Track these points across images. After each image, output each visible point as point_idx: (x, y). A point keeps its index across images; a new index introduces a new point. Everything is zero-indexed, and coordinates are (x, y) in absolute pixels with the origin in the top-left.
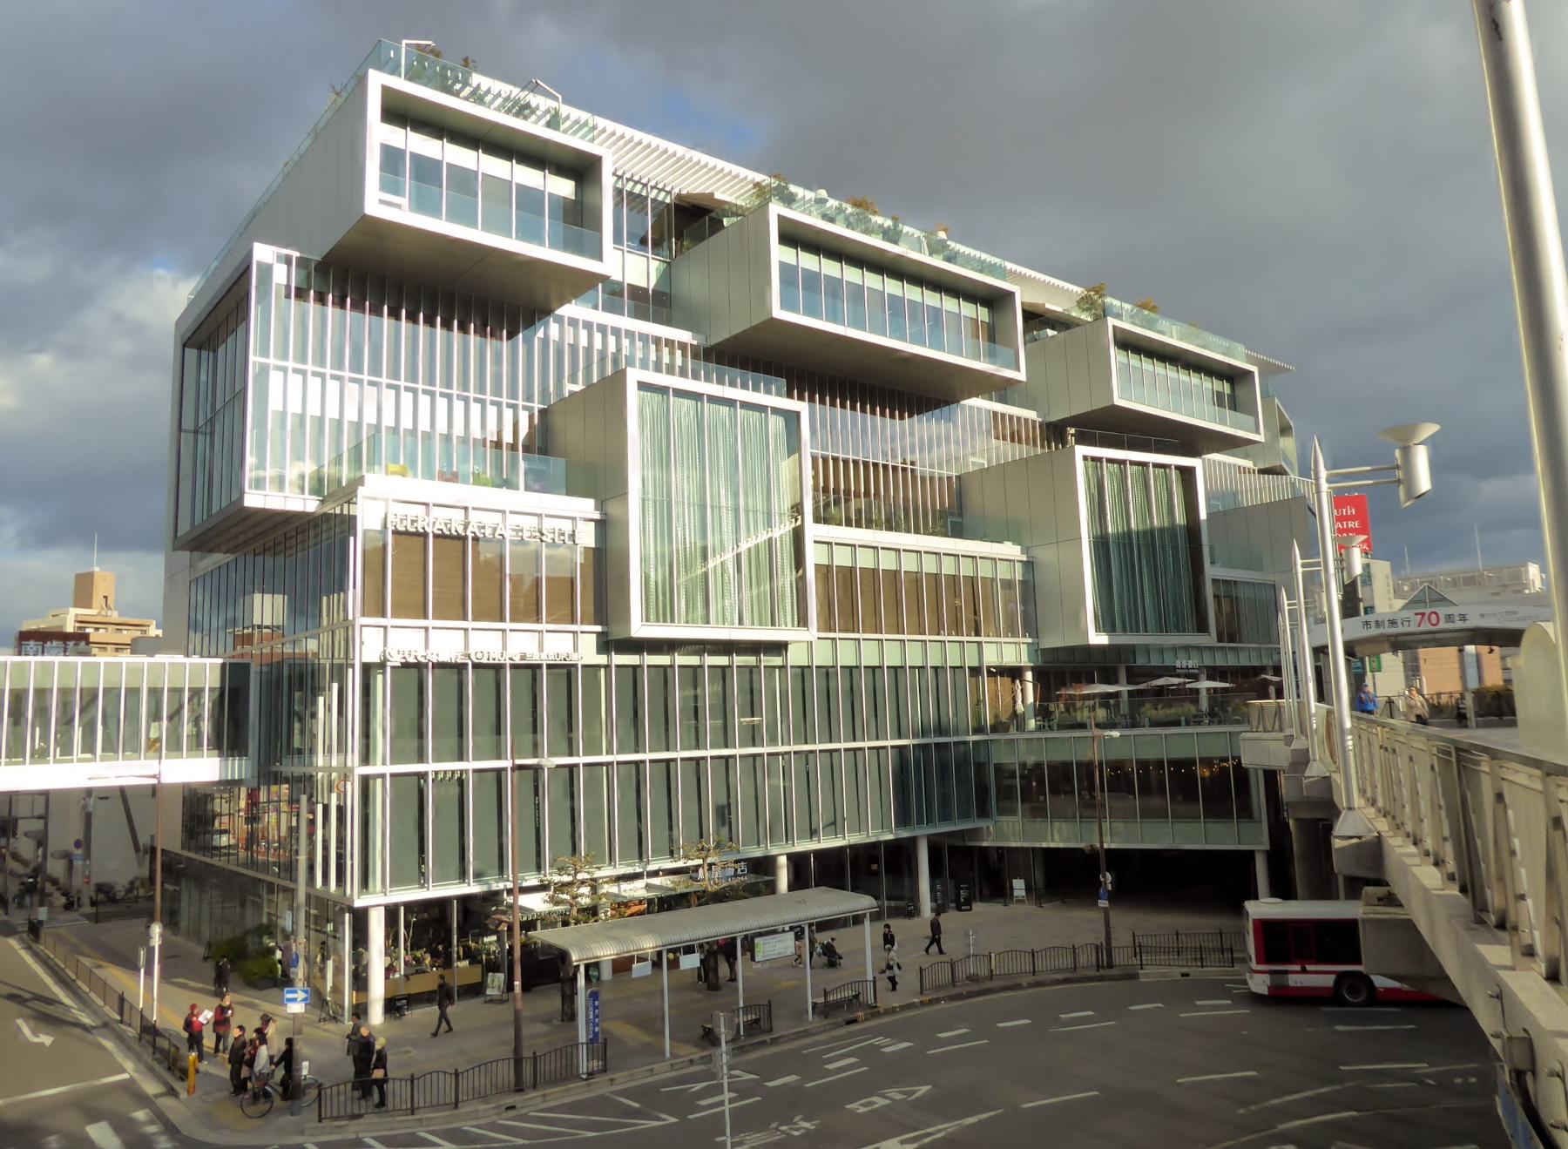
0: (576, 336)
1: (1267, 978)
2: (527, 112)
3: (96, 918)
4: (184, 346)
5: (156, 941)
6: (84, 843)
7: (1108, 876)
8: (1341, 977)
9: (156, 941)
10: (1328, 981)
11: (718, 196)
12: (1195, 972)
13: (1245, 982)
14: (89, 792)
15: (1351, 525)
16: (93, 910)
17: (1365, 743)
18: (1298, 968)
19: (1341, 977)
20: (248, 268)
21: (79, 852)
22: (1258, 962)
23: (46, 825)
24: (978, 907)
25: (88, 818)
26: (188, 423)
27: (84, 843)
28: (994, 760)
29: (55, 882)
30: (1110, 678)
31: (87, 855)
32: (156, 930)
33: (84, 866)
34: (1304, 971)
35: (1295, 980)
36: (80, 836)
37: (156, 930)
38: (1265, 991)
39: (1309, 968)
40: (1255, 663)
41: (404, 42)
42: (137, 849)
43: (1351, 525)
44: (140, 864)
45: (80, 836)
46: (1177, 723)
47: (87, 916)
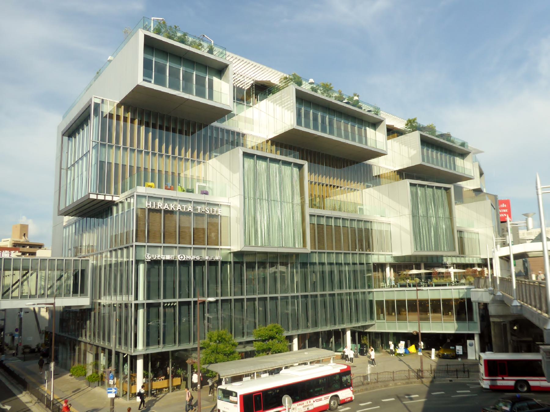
0: (218, 134)
1: (489, 382)
2: (200, 47)
3: (25, 359)
4: (63, 135)
5: (52, 369)
6: (19, 330)
7: (422, 343)
8: (517, 381)
9: (52, 369)
10: (512, 383)
11: (272, 81)
12: (455, 380)
13: (479, 384)
14: (21, 309)
15: (504, 211)
16: (23, 356)
17: (14, 287)
18: (501, 378)
19: (517, 381)
20: (89, 106)
21: (17, 333)
22: (486, 376)
23: (5, 322)
24: (487, 353)
25: (21, 319)
26: (64, 166)
27: (19, 330)
28: (375, 299)
29: (7, 345)
30: (418, 267)
31: (20, 334)
32: (52, 365)
33: (19, 339)
34: (503, 379)
35: (500, 383)
36: (18, 327)
37: (52, 365)
38: (488, 387)
39: (505, 378)
40: (471, 262)
41: (152, 18)
42: (40, 333)
43: (504, 211)
44: (41, 338)
45: (18, 327)
46: (445, 285)
47: (20, 358)
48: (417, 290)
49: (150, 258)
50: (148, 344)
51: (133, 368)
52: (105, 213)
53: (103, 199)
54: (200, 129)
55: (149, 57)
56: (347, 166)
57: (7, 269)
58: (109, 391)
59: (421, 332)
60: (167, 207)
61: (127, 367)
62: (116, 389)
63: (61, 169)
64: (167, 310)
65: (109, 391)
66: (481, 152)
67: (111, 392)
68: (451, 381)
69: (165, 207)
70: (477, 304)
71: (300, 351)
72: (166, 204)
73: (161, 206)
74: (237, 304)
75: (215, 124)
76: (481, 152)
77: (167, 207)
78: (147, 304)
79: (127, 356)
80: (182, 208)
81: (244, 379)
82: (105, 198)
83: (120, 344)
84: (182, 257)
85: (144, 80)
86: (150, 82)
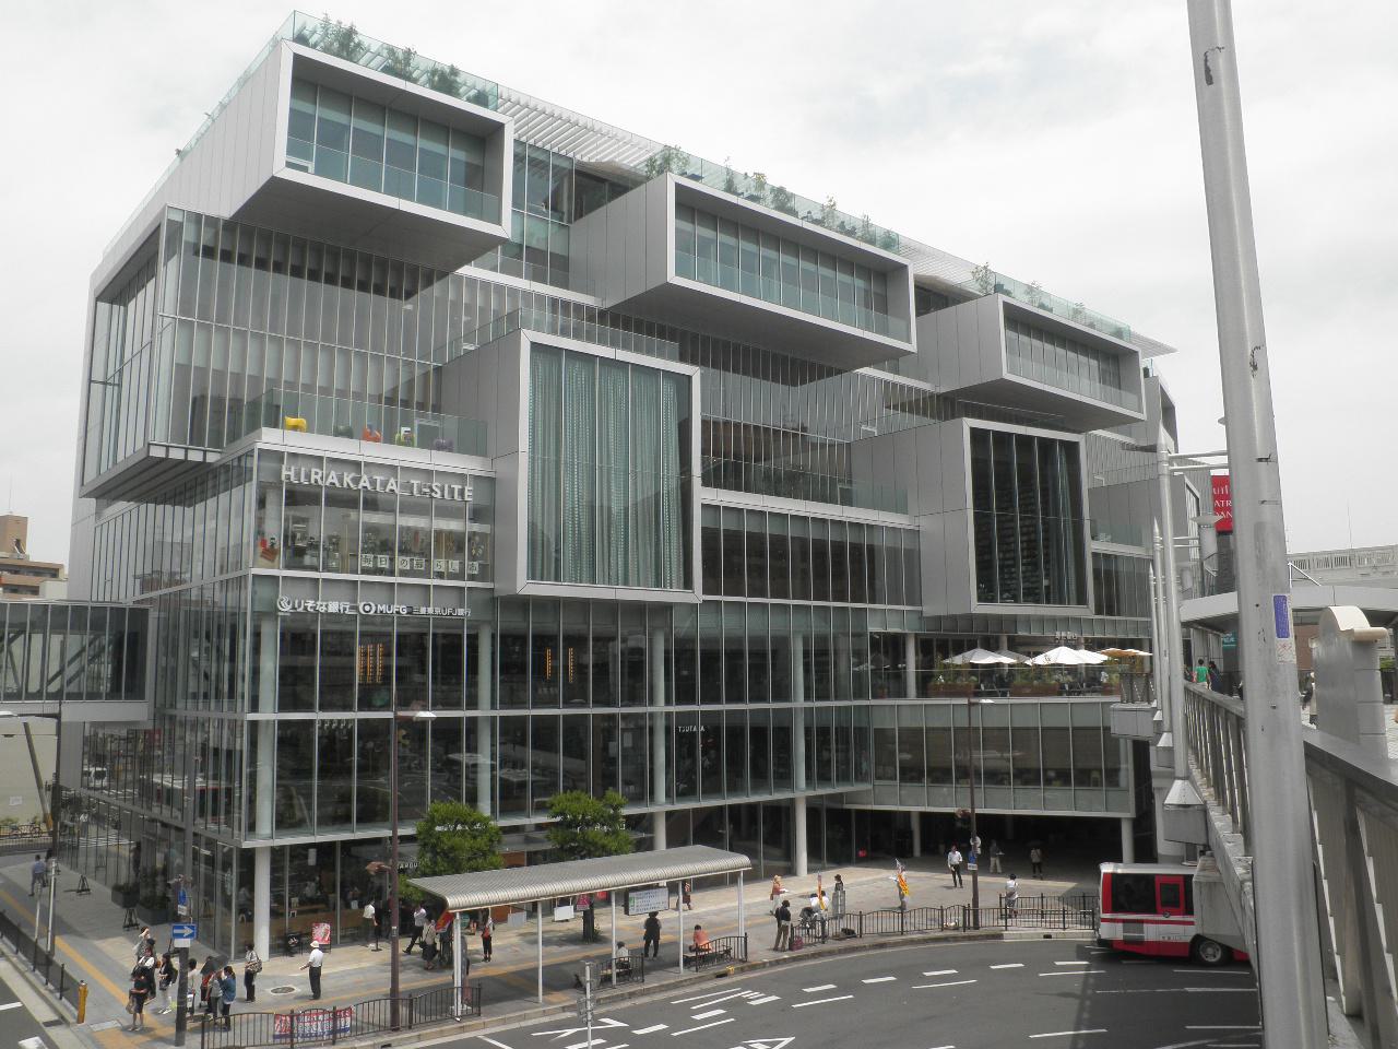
0: (473, 297)
4: (98, 299)
7: (979, 840)
48: (970, 704)
49: (288, 608)
50: (283, 822)
51: (247, 881)
52: (199, 489)
53: (182, 457)
54: (429, 283)
55: (306, 107)
56: (803, 382)
57: (20, 630)
58: (176, 931)
59: (978, 811)
60: (335, 481)
61: (232, 877)
62: (192, 928)
63: (90, 381)
64: (57, 711)
65: (176, 931)
66: (1169, 350)
67: (181, 936)
68: (1048, 936)
69: (330, 480)
70: (1130, 744)
71: (674, 850)
72: (333, 473)
73: (318, 477)
74: (626, 734)
75: (467, 271)
76: (1169, 350)
77: (335, 481)
78: (359, 720)
79: (231, 850)
80: (373, 482)
81: (511, 917)
82: (186, 455)
83: (202, 813)
84: (367, 608)
85: (289, 165)
86: (305, 169)
